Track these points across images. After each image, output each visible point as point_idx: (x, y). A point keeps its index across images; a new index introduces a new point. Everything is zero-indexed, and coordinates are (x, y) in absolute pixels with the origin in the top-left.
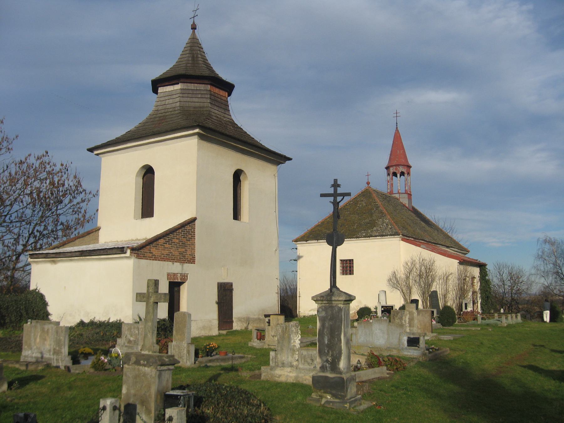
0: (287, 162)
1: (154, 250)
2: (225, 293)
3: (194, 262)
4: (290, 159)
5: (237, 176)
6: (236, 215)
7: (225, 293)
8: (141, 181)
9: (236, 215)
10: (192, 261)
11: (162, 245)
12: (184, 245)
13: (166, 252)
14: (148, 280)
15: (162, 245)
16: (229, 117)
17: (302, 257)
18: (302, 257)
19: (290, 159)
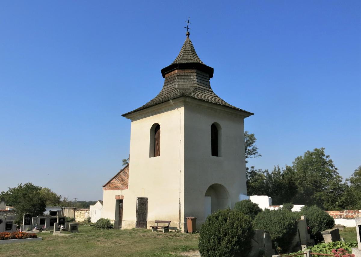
0: (251, 116)
1: (111, 186)
2: (142, 203)
3: (127, 188)
4: (252, 114)
5: (215, 129)
6: (215, 152)
7: (142, 203)
8: (218, 133)
9: (215, 152)
10: (126, 187)
11: (114, 182)
12: (123, 180)
13: (115, 185)
14: (148, 198)
15: (114, 182)
16: (210, 90)
17: (102, 186)
18: (102, 186)
19: (252, 114)
